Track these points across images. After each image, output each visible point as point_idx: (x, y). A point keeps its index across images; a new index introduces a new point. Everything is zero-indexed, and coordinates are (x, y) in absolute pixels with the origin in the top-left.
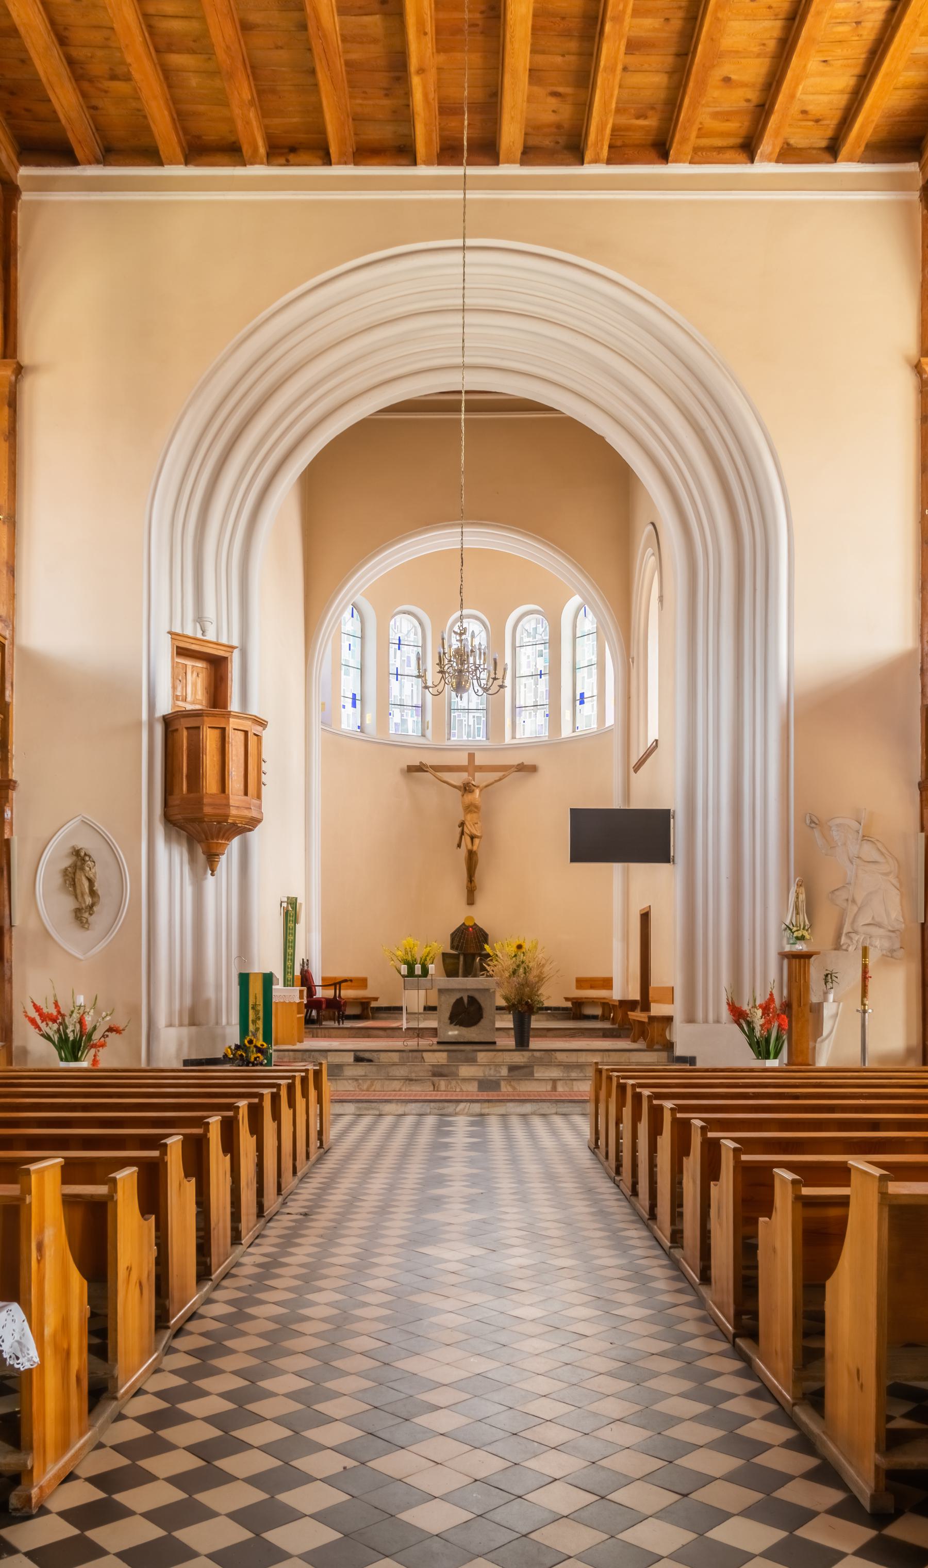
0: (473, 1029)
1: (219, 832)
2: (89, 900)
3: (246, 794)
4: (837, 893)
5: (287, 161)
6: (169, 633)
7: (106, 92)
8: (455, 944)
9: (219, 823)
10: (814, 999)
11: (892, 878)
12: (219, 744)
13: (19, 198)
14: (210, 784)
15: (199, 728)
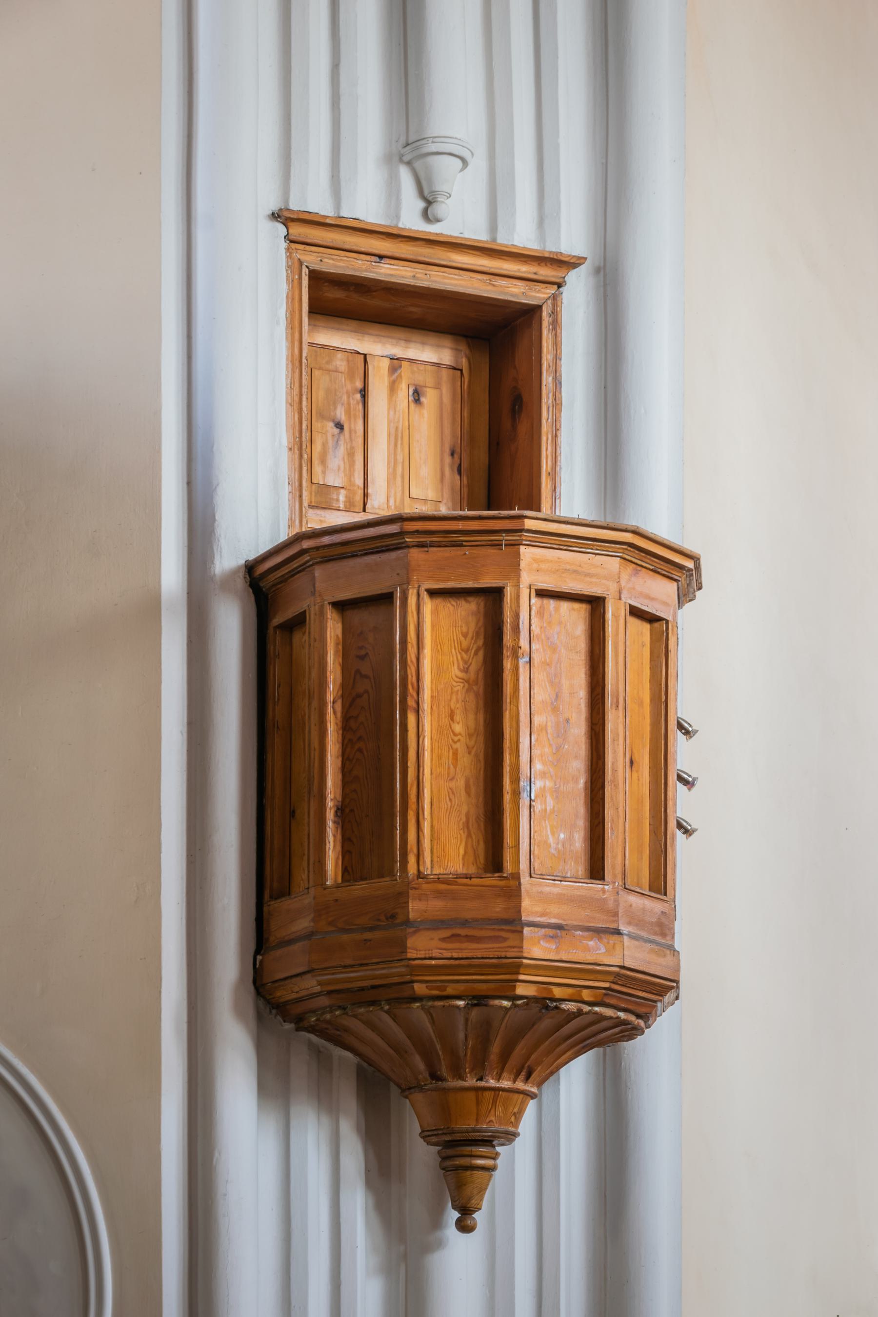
1: (485, 1041)
3: (596, 870)
6: (275, 216)
9: (479, 1000)
12: (477, 662)
14: (438, 837)
15: (388, 598)
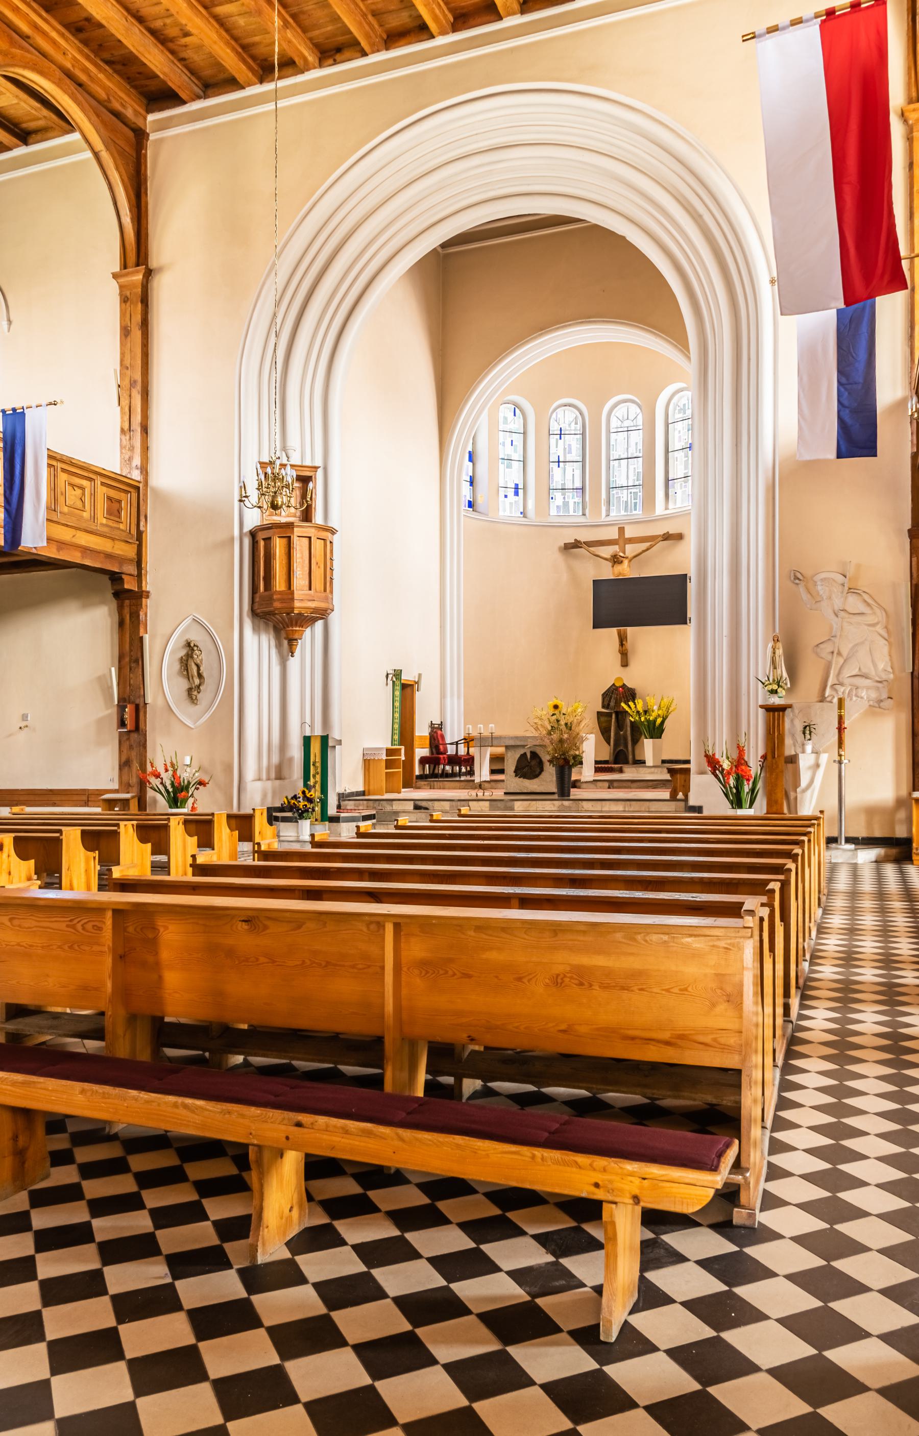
0: (535, 781)
2: (197, 681)
4: (821, 646)
5: (335, 60)
7: (186, 46)
8: (606, 703)
10: (789, 751)
11: (879, 628)
13: (148, 139)
14: (279, 584)
